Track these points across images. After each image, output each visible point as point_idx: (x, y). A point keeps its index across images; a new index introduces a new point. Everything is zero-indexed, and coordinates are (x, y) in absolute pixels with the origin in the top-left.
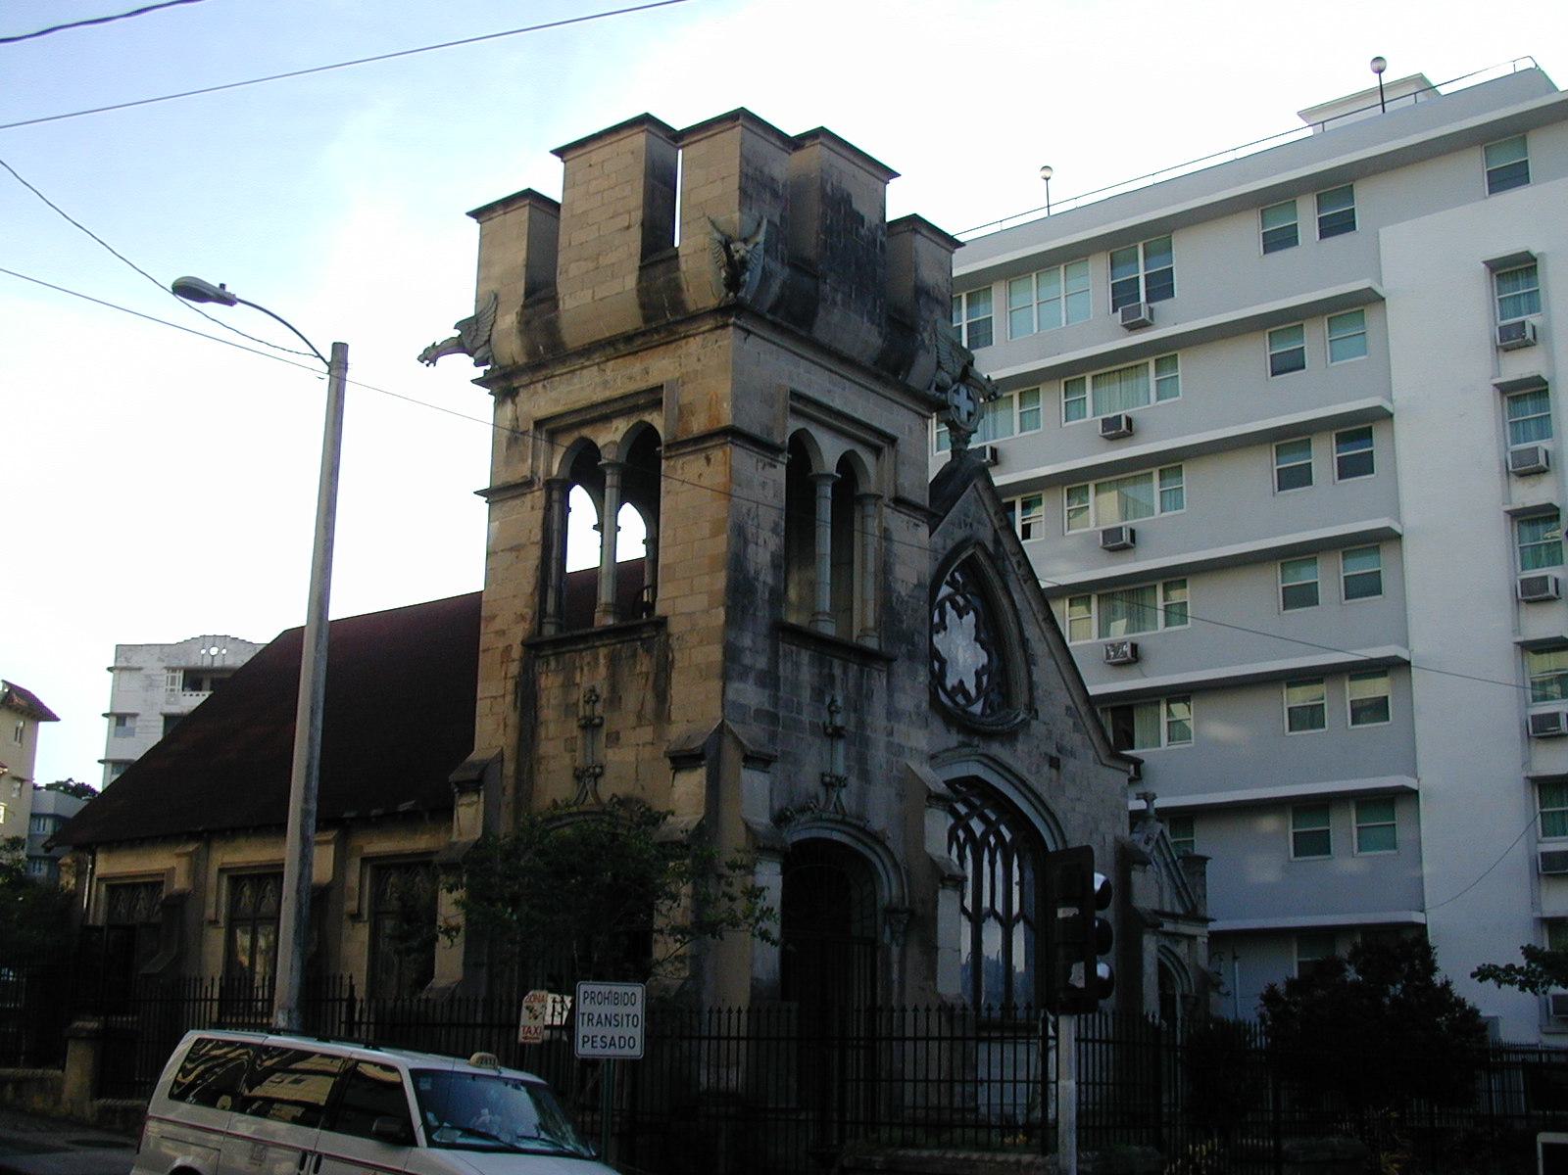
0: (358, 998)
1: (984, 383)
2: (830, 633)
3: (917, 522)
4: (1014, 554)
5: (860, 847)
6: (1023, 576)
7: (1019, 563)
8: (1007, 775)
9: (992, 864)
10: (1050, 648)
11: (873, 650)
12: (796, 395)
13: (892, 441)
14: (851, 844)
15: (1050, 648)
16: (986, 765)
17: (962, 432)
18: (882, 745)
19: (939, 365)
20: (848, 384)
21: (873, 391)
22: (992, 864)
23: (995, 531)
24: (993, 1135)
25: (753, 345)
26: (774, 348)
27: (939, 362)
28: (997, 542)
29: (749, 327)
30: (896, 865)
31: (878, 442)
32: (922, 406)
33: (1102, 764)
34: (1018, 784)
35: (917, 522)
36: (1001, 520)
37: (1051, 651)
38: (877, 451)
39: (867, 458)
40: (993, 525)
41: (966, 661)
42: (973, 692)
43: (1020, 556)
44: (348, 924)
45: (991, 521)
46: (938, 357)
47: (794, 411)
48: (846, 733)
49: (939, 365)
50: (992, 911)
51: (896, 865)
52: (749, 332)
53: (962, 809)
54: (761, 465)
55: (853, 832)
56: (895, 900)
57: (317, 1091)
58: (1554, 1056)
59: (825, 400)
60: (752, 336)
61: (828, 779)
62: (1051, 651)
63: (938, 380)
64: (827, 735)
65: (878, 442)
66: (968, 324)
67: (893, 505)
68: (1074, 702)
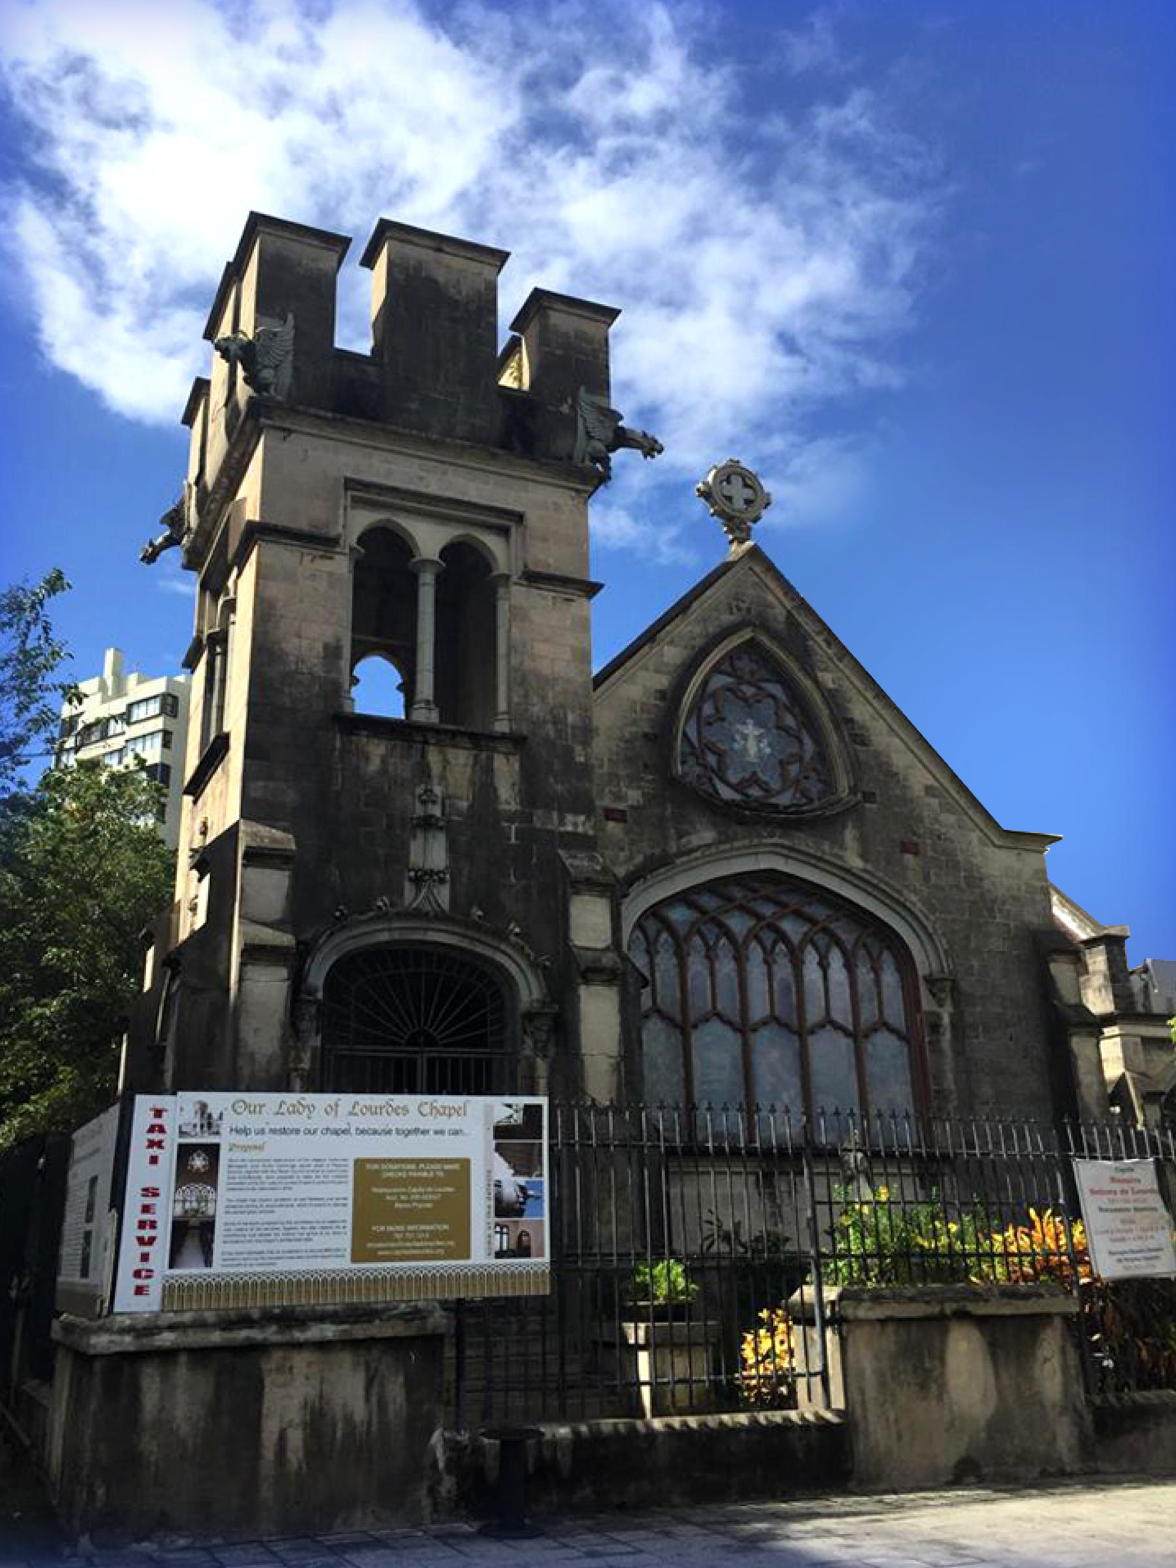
2: (397, 716)
4: (818, 634)
9: (824, 966)
10: (888, 724)
12: (349, 484)
13: (519, 518)
14: (461, 944)
15: (888, 724)
19: (590, 437)
22: (824, 966)
23: (788, 612)
24: (683, 1285)
25: (298, 443)
26: (331, 443)
27: (588, 433)
29: (287, 425)
33: (995, 846)
34: (842, 874)
38: (504, 532)
39: (493, 542)
41: (760, 750)
43: (826, 633)
45: (781, 603)
47: (355, 500)
50: (828, 1022)
52: (290, 431)
53: (768, 910)
54: (307, 559)
57: (427, 1235)
59: (422, 489)
60: (293, 435)
67: (524, 582)
68: (937, 780)
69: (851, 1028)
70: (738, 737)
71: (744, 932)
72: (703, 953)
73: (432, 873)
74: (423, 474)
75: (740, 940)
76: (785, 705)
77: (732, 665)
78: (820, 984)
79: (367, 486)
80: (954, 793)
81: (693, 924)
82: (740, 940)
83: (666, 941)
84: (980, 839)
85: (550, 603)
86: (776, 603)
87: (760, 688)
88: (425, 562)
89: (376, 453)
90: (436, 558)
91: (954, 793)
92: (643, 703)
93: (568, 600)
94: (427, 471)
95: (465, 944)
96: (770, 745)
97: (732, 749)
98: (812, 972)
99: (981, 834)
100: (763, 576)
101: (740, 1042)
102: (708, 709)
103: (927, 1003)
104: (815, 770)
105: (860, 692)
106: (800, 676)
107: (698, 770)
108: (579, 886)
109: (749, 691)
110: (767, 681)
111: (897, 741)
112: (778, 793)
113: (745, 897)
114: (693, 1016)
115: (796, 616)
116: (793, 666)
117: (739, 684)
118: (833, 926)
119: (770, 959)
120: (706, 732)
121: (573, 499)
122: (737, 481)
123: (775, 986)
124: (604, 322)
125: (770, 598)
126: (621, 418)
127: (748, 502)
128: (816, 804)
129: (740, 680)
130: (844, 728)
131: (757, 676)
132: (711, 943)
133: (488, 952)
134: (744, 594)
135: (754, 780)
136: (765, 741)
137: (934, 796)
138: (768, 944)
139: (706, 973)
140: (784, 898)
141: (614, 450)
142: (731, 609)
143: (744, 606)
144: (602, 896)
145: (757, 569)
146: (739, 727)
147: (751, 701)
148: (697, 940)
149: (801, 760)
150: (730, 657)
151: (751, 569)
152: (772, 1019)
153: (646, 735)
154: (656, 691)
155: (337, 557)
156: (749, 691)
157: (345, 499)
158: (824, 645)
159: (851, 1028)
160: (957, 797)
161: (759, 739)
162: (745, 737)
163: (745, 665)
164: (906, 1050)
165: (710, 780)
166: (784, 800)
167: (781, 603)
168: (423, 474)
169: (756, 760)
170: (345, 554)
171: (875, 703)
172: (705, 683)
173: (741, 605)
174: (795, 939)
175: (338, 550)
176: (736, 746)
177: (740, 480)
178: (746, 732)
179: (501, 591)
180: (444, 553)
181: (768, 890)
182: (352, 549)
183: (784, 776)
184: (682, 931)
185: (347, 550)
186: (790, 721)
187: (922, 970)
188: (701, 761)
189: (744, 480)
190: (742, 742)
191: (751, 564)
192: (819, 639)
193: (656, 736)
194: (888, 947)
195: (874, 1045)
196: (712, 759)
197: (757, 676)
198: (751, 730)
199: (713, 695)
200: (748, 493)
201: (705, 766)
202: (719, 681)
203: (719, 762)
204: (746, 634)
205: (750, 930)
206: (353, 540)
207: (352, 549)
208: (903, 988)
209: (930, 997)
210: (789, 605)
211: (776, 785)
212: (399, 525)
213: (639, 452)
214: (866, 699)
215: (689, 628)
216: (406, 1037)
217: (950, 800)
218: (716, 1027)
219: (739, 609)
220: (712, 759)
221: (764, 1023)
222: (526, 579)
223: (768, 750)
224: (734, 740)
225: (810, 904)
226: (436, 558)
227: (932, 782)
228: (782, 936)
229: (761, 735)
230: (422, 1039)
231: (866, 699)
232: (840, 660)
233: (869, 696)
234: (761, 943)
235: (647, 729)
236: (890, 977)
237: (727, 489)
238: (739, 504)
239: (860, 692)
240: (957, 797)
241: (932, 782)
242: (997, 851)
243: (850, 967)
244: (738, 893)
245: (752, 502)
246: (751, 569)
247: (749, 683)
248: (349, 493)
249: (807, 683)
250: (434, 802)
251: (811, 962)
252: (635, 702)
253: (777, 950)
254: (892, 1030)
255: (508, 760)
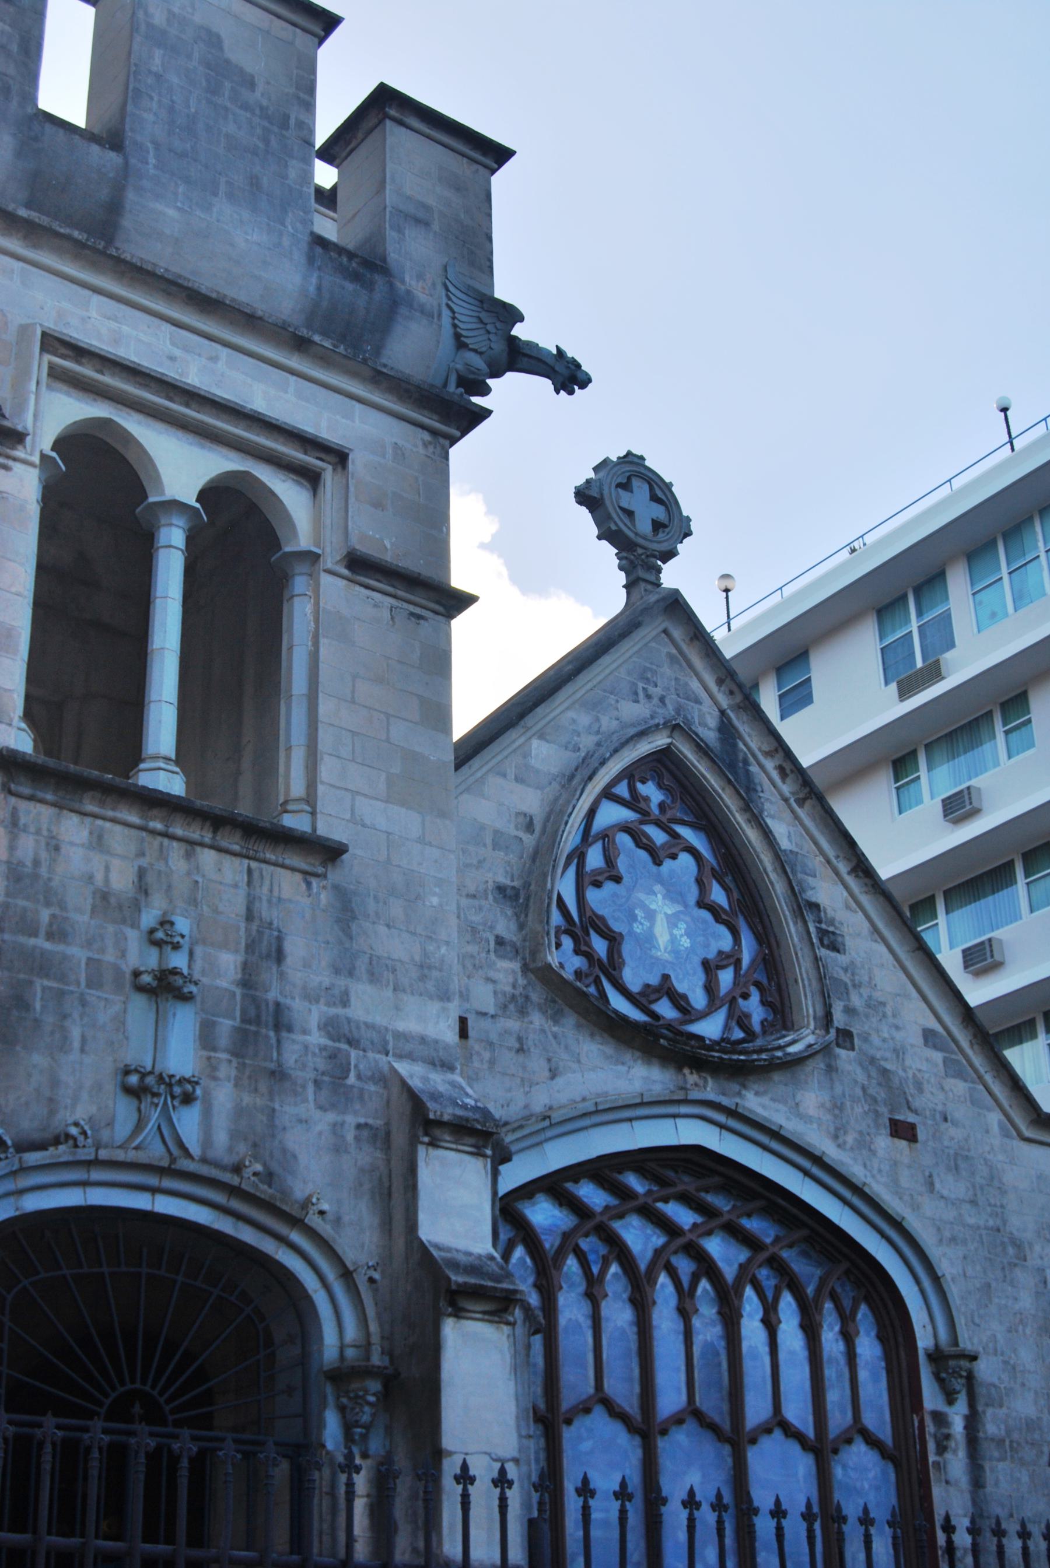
0: (851, 1510)
1: (551, 362)
3: (418, 610)
4: (768, 754)
5: (247, 1235)
6: (793, 793)
7: (781, 769)
8: (775, 1145)
9: (770, 1324)
11: (179, 797)
12: (51, 342)
13: (340, 457)
14: (216, 1226)
16: (722, 1126)
17: (640, 551)
18: (48, 946)
20: (224, 352)
21: (292, 372)
22: (770, 1324)
23: (723, 712)
26: (17, 265)
27: (457, 336)
28: (726, 729)
30: (347, 1275)
31: (310, 460)
32: (426, 412)
35: (418, 610)
36: (731, 693)
37: (875, 930)
38: (311, 479)
40: (716, 703)
41: (673, 940)
42: (698, 999)
43: (779, 757)
44: (831, 1455)
45: (711, 696)
46: (455, 326)
47: (56, 375)
48: (193, 989)
49: (460, 344)
50: (779, 1423)
51: (347, 1275)
53: (684, 1217)
55: (219, 1198)
56: (350, 1353)
58: (100, 247)
61: (134, 1079)
62: (875, 930)
63: (459, 367)
64: (141, 989)
65: (310, 460)
66: (919, 627)
67: (346, 572)
69: (811, 1433)
70: (639, 913)
71: (649, 1254)
72: (582, 1288)
73: (167, 1081)
74: (177, 352)
75: (643, 1266)
76: (713, 869)
77: (632, 789)
78: (764, 1350)
79: (79, 352)
80: (965, 1044)
81: (566, 1236)
82: (643, 1266)
83: (522, 1260)
84: (1000, 1123)
85: (386, 614)
86: (704, 695)
87: (675, 835)
88: (176, 506)
89: (96, 299)
90: (192, 501)
91: (965, 1044)
92: (496, 832)
93: (419, 617)
94: (186, 349)
95: (225, 1225)
96: (688, 934)
97: (631, 932)
98: (752, 1330)
99: (1003, 1118)
100: (684, 647)
101: (639, 1452)
102: (594, 858)
103: (931, 1397)
104: (757, 984)
105: (829, 862)
106: (740, 819)
107: (578, 962)
108: (437, 1132)
109: (658, 837)
110: (683, 823)
111: (883, 949)
112: (703, 1015)
113: (649, 1192)
114: (568, 1400)
115: (736, 722)
116: (729, 801)
117: (642, 822)
118: (785, 1254)
119: (688, 1306)
120: (593, 896)
121: (425, 445)
122: (641, 490)
123: (696, 1350)
124: (486, 167)
125: (695, 685)
126: (520, 318)
127: (657, 526)
128: (759, 1042)
129: (645, 815)
130: (810, 918)
131: (669, 814)
132: (595, 1270)
133: (268, 1246)
134: (655, 673)
135: (666, 989)
136: (683, 926)
137: (935, 1047)
138: (685, 1280)
139: (586, 1324)
140: (710, 1198)
141: (497, 374)
142: (636, 693)
143: (656, 692)
144: (478, 1154)
145: (677, 633)
146: (642, 896)
147: (662, 854)
148: (571, 1264)
149: (738, 963)
150: (630, 774)
151: (665, 631)
152: (693, 1413)
153: (501, 889)
154: (518, 814)
155: (18, 467)
156: (658, 837)
157: (39, 363)
158: (775, 775)
159: (811, 1433)
160: (970, 1052)
161: (672, 921)
162: (651, 915)
163: (652, 792)
164: (892, 1477)
165: (597, 982)
166: (710, 1028)
167: (711, 696)
168: (177, 352)
169: (667, 956)
170: (32, 464)
171: (850, 880)
172: (592, 813)
173: (652, 690)
174: (729, 1273)
175: (19, 453)
176: (637, 928)
177: (646, 487)
178: (653, 907)
179: (300, 584)
180: (203, 495)
181: (687, 1183)
182: (43, 457)
183: (710, 988)
184: (550, 1243)
185: (36, 459)
186: (718, 895)
187: (924, 1341)
188: (584, 948)
189: (651, 489)
190: (647, 924)
191: (666, 624)
192: (770, 765)
193: (516, 890)
194: (868, 1300)
195: (845, 1467)
196: (600, 946)
197: (669, 814)
198: (660, 905)
199: (605, 836)
200: (658, 512)
201: (589, 955)
202: (611, 814)
203: (611, 952)
204: (661, 741)
205: (658, 1252)
206: (46, 443)
207: (43, 457)
208: (889, 1371)
209: (936, 1385)
210: (724, 701)
211: (698, 999)
212: (128, 438)
213: (546, 384)
214: (837, 873)
215: (571, 714)
216: (108, 1402)
217: (960, 1057)
218: (599, 1421)
219: (649, 697)
220: (600, 946)
221: (678, 1420)
222: (349, 567)
223: (686, 942)
224: (634, 918)
225: (749, 1215)
226: (192, 501)
227: (933, 1024)
228: (707, 1267)
229: (676, 915)
230: (137, 1409)
231: (837, 873)
232: (801, 802)
233: (843, 868)
234: (673, 1273)
235: (503, 880)
236: (868, 1347)
237: (626, 499)
238: (644, 526)
239: (829, 862)
240: (970, 1052)
241: (933, 1024)
242: (1025, 1147)
243: (811, 1330)
244: (635, 1183)
245: (665, 526)
246: (665, 631)
247: (658, 824)
248: (47, 357)
249: (752, 835)
250: (176, 947)
251: (750, 1315)
252: (483, 828)
253: (699, 1291)
254: (872, 1441)
255: (309, 884)
